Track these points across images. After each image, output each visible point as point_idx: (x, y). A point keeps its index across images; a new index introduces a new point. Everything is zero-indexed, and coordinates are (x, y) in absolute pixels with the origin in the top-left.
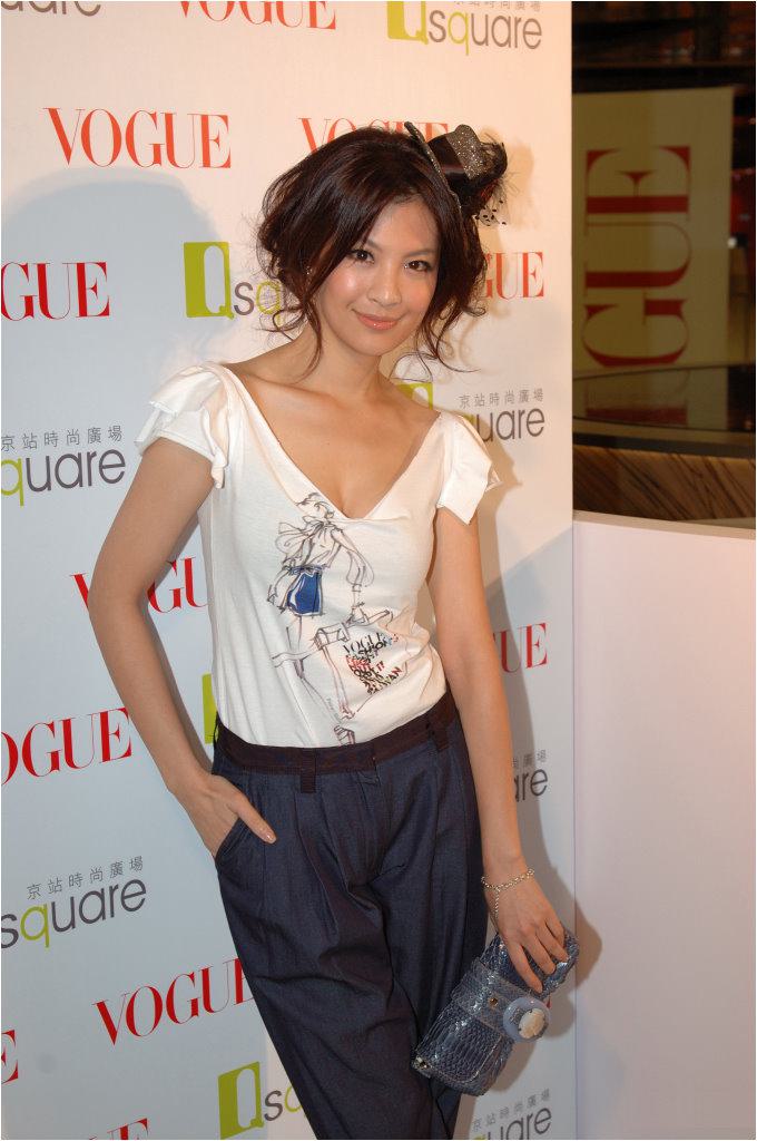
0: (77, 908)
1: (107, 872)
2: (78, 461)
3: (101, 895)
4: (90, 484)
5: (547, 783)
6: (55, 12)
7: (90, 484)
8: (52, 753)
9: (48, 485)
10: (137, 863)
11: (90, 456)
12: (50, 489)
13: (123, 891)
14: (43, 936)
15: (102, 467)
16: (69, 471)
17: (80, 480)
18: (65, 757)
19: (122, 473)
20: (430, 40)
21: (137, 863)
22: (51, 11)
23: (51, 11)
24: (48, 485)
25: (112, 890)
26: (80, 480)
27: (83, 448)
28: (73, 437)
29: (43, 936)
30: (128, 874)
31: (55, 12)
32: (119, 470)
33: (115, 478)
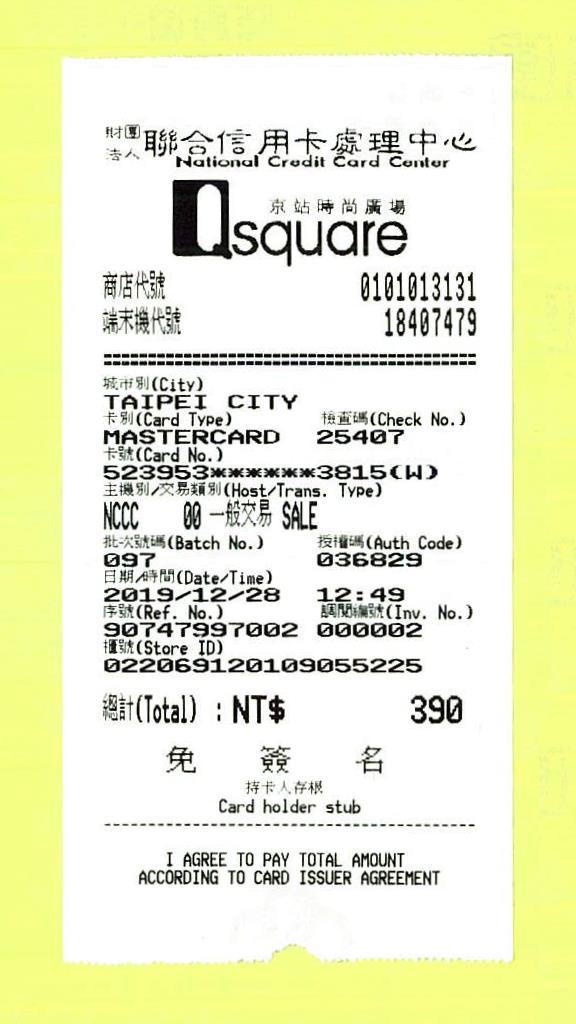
0: (325, 237)
1: (362, 207)
3: (353, 227)
5: (134, 568)
6: (355, 254)
9: (318, 250)
10: (398, 207)
11: (367, 226)
12: (320, 254)
14: (286, 253)
15: (380, 238)
19: (404, 245)
21: (398, 207)
22: (352, 253)
23: (352, 253)
24: (318, 250)
25: (367, 226)
26: (353, 249)
27: (361, 217)
28: (349, 207)
29: (285, 254)
30: (386, 215)
31: (355, 254)
32: (400, 242)
33: (395, 248)
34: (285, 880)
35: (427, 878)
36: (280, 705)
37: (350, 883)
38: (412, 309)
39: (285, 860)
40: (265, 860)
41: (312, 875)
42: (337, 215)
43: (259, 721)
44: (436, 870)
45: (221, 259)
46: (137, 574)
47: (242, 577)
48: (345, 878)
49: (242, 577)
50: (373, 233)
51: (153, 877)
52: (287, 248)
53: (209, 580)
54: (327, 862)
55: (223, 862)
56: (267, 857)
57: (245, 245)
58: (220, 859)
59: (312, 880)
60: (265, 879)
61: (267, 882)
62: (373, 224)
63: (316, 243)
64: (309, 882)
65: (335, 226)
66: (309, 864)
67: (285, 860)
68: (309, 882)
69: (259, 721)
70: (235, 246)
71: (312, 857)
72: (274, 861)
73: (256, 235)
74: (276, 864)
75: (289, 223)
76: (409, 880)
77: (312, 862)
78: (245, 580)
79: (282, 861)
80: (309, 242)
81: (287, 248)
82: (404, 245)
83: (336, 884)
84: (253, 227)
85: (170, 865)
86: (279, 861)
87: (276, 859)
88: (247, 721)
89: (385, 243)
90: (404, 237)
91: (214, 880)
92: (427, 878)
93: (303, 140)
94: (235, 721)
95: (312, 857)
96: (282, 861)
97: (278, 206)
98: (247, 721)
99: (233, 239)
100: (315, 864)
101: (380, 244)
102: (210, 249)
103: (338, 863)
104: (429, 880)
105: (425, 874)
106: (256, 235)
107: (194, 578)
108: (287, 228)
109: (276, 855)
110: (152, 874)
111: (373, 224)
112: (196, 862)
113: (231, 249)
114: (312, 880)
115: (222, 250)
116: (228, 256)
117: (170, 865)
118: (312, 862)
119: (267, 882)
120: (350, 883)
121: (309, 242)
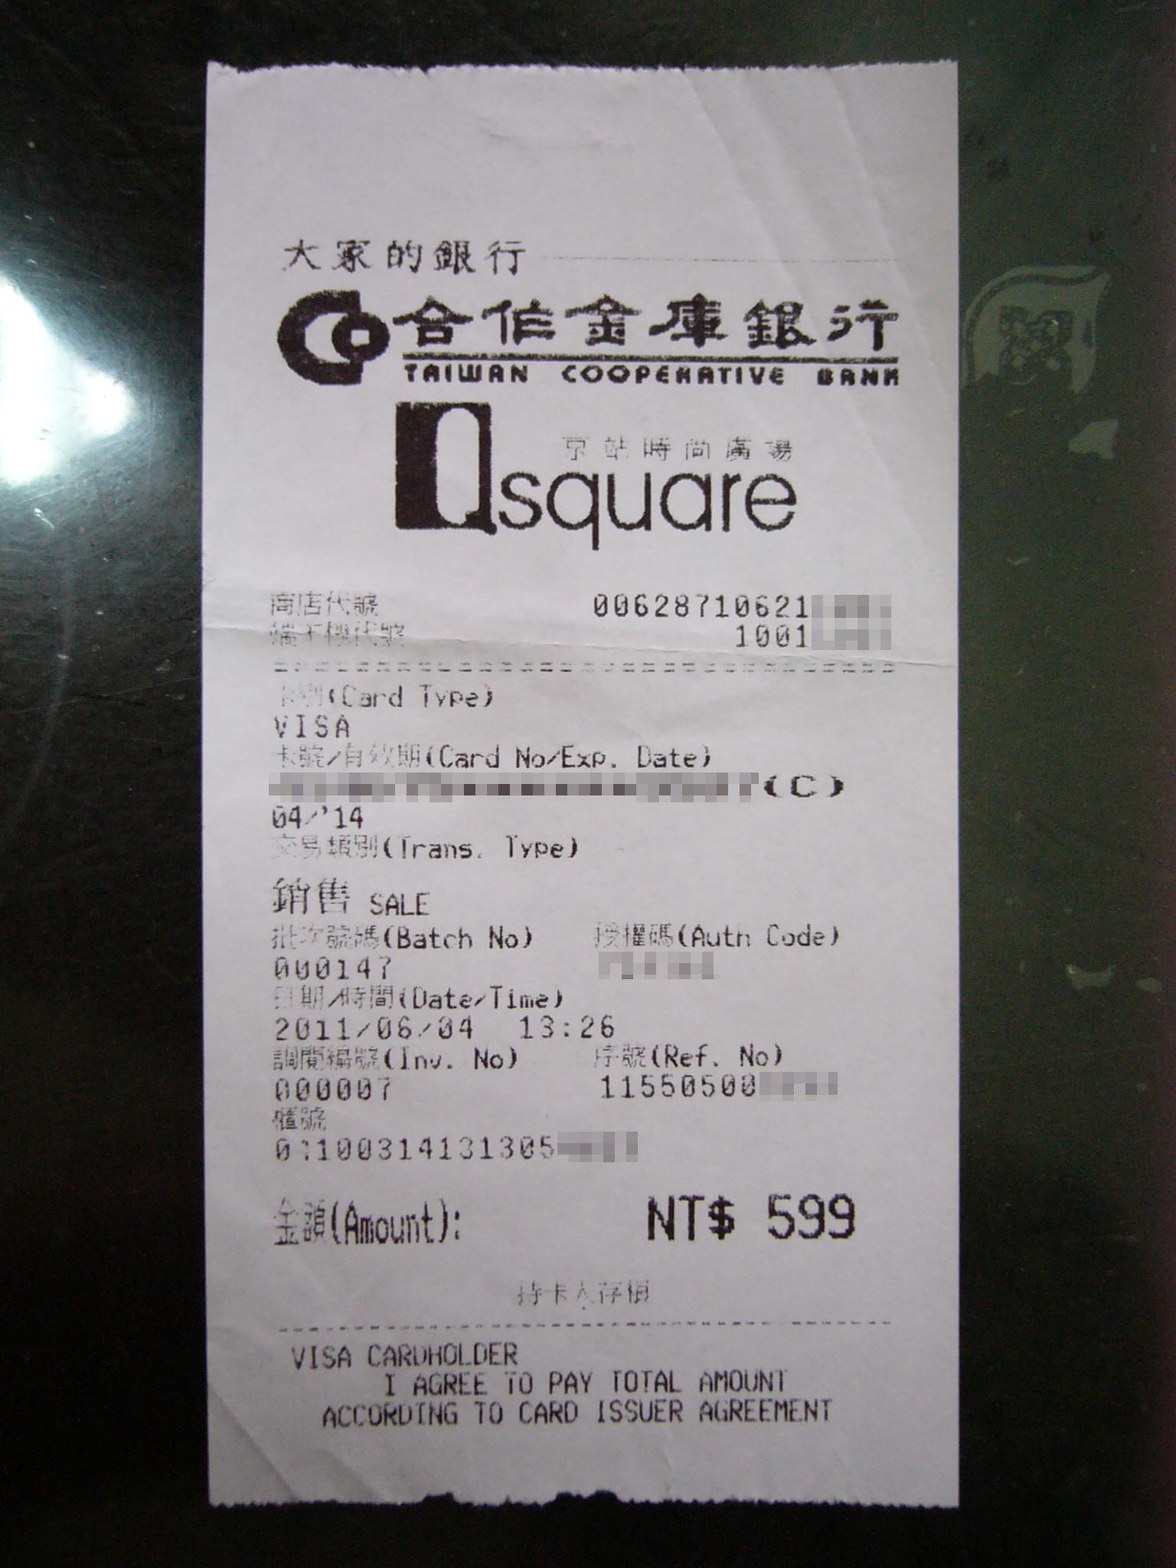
1: (720, 446)
2: (706, 485)
4: (726, 528)
6: (708, 528)
7: (726, 528)
8: (836, 1093)
9: (645, 522)
10: (783, 449)
11: (729, 482)
12: (648, 527)
13: (750, 491)
14: (590, 526)
15: (749, 503)
16: (687, 502)
17: (705, 519)
18: (811, 1089)
19: (790, 516)
20: (489, 1065)
22: (704, 526)
23: (704, 526)
25: (729, 482)
26: (705, 519)
27: (717, 467)
29: (590, 526)
31: (708, 528)
33: (775, 521)
34: (571, 1416)
35: (811, 1411)
36: (716, 1223)
37: (680, 1420)
38: (725, 333)
39: (586, 1384)
40: (552, 1384)
41: (616, 1406)
42: (677, 463)
43: (691, 1237)
44: (826, 1397)
45: (479, 534)
46: (330, 994)
47: (511, 997)
48: (672, 1412)
49: (511, 997)
50: (738, 492)
51: (347, 1416)
52: (593, 518)
53: (455, 1002)
54: (657, 1384)
55: (480, 1388)
56: (556, 1378)
57: (520, 513)
58: (477, 1384)
59: (616, 1416)
60: (537, 1415)
61: (541, 1419)
62: (737, 478)
63: (643, 509)
64: (613, 1419)
65: (675, 480)
66: (627, 1387)
67: (586, 1384)
68: (613, 1419)
69: (691, 1237)
70: (503, 517)
71: (631, 1377)
72: (567, 1386)
73: (539, 496)
74: (571, 1390)
75: (596, 477)
76: (781, 1413)
77: (631, 1385)
78: (517, 1002)
79: (581, 1386)
80: (630, 508)
81: (593, 518)
82: (790, 516)
83: (658, 1420)
84: (534, 482)
85: (390, 1393)
86: (575, 1385)
87: (571, 1381)
88: (671, 1237)
89: (757, 509)
90: (791, 500)
91: (451, 1418)
92: (811, 1411)
93: (722, 611)
94: (651, 1237)
95: (631, 1377)
96: (581, 1386)
97: (577, 444)
98: (671, 1237)
99: (498, 502)
100: (635, 1388)
101: (749, 511)
102: (462, 520)
103: (675, 1387)
104: (815, 1414)
105: (807, 1405)
106: (539, 496)
107: (429, 1000)
108: (593, 484)
109: (571, 1375)
110: (344, 1411)
111: (737, 478)
112: (435, 1389)
113: (495, 518)
114: (616, 1416)
115: (480, 520)
116: (491, 529)
117: (390, 1393)
118: (631, 1385)
119: (541, 1419)
120: (680, 1420)
121: (630, 508)
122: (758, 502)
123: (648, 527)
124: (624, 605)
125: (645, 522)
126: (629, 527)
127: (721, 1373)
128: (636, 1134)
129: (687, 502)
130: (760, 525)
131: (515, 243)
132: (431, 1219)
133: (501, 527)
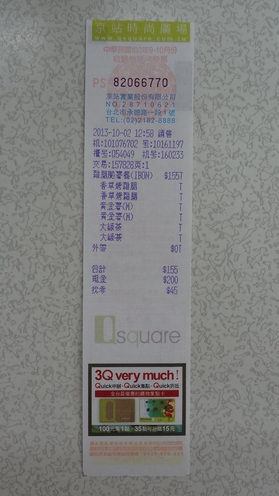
2: (161, 334)
7: (165, 343)
9: (148, 341)
11: (166, 333)
12: (148, 343)
13: (171, 334)
15: (170, 337)
16: (157, 337)
26: (161, 340)
50: (168, 335)
62: (168, 332)
70: (117, 340)
82: (179, 340)
90: (179, 337)
101: (170, 339)
111: (168, 332)
121: (145, 338)
122: (173, 337)
123: (148, 343)
124: (157, 49)
125: (148, 341)
126: (145, 343)
127: (168, 130)
128: (148, 379)
129: (157, 337)
130: (172, 342)
131: (136, 83)
132: (112, 380)
133: (117, 343)
